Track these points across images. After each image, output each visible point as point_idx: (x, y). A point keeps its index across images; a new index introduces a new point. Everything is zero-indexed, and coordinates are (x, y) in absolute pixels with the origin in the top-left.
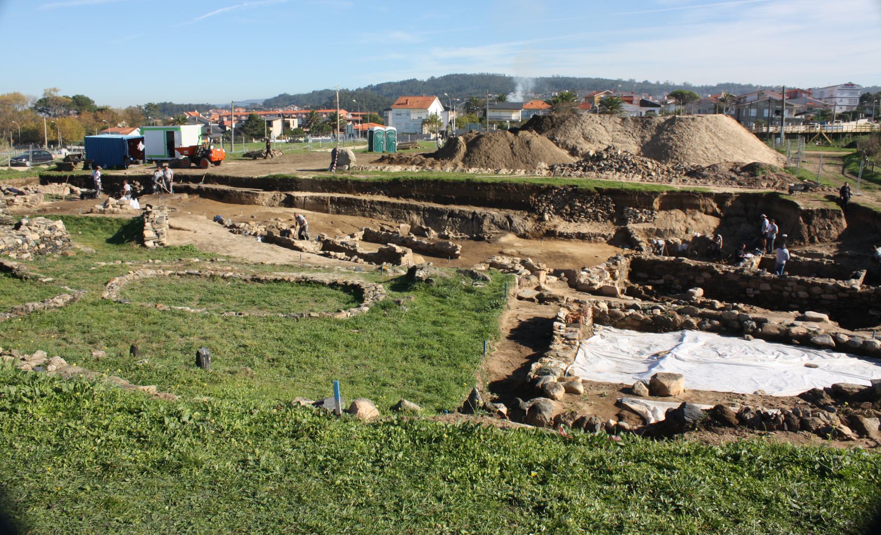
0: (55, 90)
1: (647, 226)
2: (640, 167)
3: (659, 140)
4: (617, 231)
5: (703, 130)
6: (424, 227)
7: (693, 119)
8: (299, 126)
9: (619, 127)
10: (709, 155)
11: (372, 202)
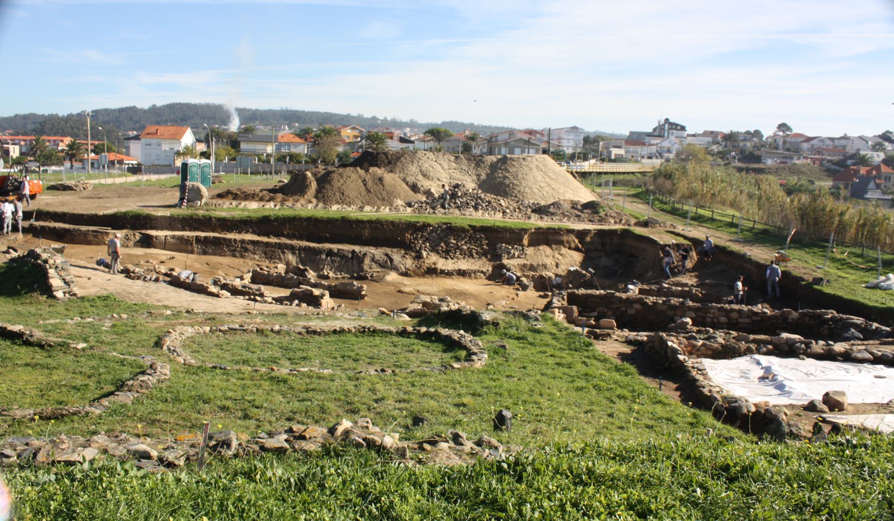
1: (521, 261)
2: (495, 204)
3: (495, 178)
4: (494, 267)
5: (535, 170)
6: (302, 267)
8: (22, 154)
9: (454, 165)
11: (243, 241)
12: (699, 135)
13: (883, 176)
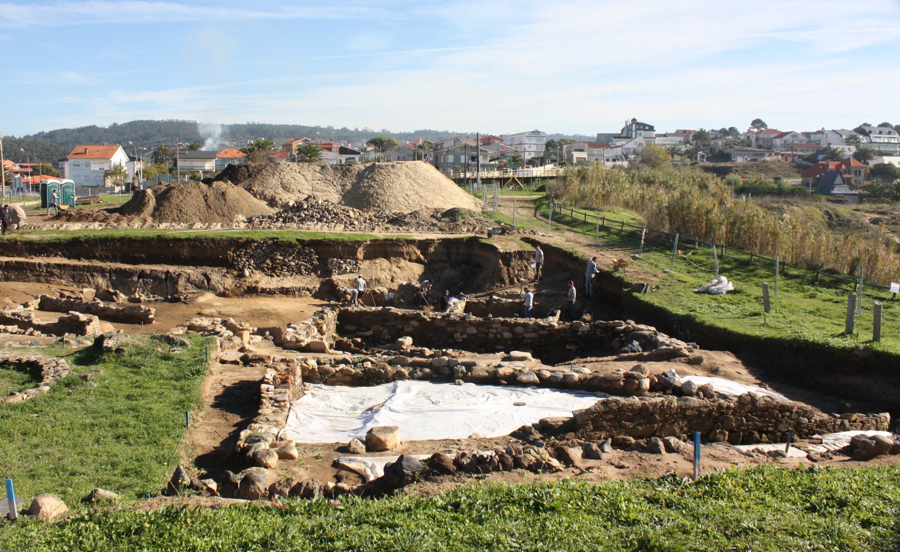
2: (342, 216)
3: (360, 188)
4: (322, 284)
5: (403, 177)
7: (393, 166)
9: (318, 175)
11: (48, 265)
12: (671, 135)
13: (853, 170)
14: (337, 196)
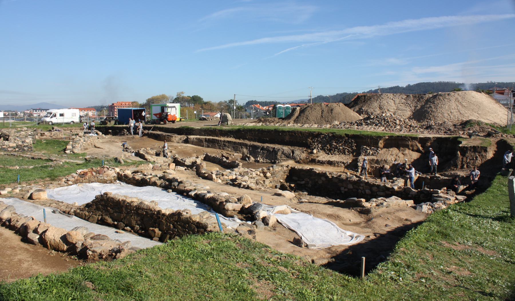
0: (182, 93)
1: (371, 157)
7: (448, 94)
9: (403, 101)
10: (452, 117)
11: (224, 141)
14: (410, 113)
